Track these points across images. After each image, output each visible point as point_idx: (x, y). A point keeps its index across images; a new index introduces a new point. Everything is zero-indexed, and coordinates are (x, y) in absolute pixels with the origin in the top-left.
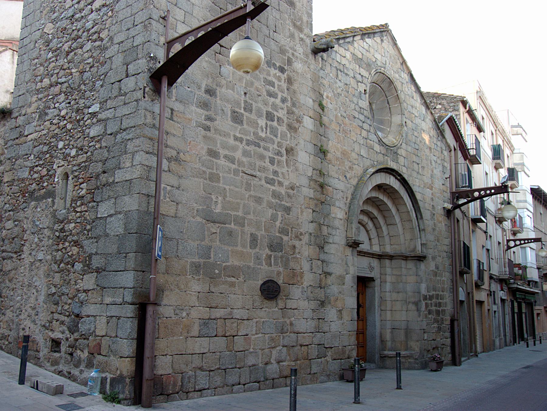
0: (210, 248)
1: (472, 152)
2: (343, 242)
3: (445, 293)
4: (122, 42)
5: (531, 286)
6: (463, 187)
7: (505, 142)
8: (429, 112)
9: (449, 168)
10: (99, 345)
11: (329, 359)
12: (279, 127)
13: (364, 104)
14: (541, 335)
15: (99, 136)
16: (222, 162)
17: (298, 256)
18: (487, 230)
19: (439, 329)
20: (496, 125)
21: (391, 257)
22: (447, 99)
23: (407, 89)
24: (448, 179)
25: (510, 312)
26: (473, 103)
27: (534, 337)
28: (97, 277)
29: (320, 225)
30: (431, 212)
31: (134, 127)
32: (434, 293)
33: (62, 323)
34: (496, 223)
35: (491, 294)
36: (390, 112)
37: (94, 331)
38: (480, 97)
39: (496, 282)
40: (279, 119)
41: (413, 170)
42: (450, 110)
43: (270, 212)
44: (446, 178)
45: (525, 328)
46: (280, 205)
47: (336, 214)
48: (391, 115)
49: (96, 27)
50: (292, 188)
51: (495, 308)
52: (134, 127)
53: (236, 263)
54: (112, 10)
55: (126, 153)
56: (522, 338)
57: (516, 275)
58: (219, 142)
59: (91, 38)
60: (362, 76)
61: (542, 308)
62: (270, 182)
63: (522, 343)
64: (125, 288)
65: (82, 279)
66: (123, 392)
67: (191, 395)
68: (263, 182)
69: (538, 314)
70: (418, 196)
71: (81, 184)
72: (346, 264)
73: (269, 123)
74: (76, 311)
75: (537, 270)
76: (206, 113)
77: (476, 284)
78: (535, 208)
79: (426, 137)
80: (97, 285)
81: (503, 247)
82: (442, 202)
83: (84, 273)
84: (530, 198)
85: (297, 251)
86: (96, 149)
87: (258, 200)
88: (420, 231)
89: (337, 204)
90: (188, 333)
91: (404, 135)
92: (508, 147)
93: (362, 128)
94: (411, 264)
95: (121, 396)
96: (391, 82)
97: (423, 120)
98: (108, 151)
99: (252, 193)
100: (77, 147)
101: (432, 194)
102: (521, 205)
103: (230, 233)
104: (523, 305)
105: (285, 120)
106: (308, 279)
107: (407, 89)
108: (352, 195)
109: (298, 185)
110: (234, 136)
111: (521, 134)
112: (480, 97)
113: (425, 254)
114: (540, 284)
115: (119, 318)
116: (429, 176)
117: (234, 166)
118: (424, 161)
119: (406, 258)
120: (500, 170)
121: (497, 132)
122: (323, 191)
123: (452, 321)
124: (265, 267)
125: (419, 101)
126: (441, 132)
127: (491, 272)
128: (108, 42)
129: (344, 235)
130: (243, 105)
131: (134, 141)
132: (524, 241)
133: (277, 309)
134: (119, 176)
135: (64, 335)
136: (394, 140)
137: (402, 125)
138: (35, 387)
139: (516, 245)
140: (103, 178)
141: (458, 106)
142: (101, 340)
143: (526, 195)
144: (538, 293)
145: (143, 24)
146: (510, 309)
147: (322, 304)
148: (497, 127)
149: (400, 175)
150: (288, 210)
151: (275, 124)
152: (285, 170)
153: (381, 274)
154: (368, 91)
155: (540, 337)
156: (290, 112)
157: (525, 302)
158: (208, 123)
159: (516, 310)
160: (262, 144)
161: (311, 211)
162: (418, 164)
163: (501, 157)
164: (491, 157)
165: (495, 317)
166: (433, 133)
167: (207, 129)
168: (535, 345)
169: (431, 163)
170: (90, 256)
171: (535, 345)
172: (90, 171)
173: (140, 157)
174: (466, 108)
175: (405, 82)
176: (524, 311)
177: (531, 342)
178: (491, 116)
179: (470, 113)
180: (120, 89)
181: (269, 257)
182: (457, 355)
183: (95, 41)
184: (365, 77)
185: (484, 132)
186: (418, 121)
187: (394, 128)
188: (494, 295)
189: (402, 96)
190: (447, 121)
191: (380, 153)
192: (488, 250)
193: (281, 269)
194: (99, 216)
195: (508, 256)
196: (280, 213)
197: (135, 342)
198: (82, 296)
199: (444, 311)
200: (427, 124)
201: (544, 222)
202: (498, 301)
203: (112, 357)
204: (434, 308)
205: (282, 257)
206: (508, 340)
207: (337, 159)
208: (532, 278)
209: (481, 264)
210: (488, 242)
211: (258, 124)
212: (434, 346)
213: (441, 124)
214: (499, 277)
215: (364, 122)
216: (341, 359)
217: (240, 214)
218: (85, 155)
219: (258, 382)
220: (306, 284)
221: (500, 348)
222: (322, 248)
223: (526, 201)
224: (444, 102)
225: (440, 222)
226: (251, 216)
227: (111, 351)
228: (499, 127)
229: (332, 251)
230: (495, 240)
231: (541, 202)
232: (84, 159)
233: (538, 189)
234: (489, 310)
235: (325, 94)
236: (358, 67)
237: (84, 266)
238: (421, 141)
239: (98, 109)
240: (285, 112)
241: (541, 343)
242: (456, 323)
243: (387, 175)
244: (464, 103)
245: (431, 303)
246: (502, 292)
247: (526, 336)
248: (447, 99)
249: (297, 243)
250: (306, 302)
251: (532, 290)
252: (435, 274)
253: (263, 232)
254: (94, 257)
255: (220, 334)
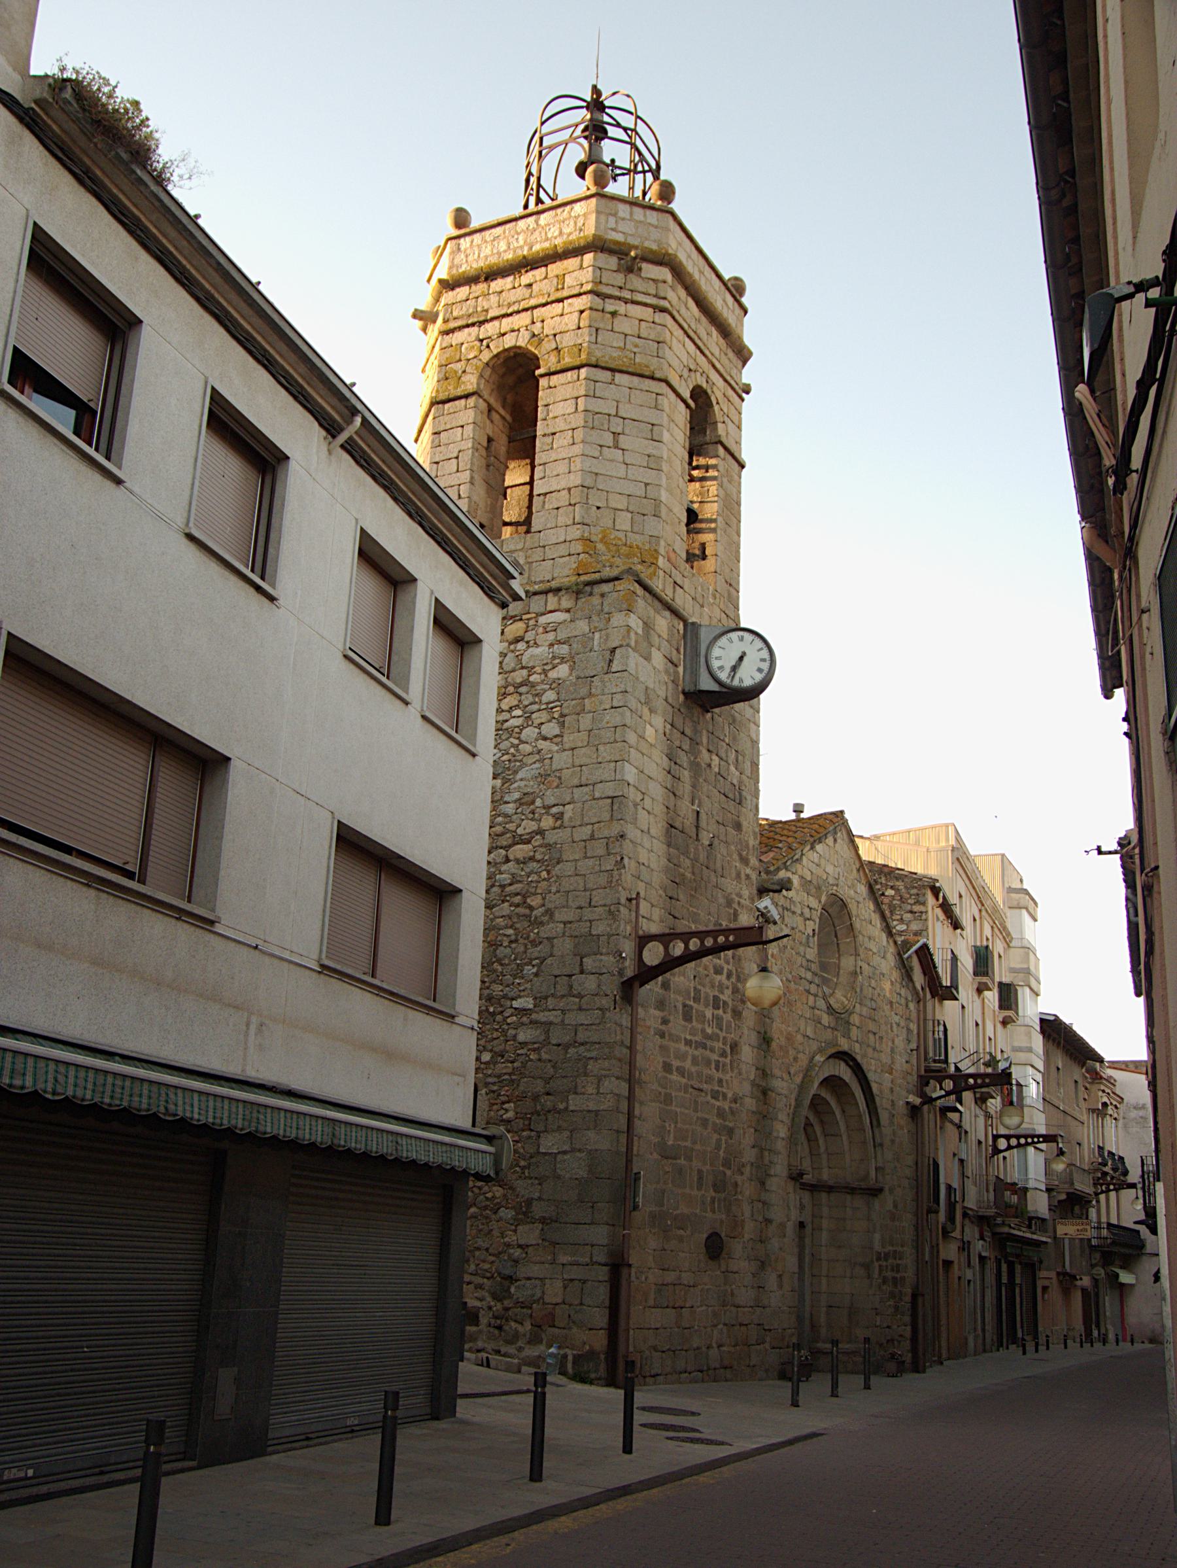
0: (663, 1192)
1: (946, 981)
2: (785, 1173)
3: (905, 1249)
4: (570, 922)
5: (1033, 1227)
6: (935, 1061)
7: (996, 930)
8: (891, 941)
9: (915, 1032)
10: (552, 1315)
11: (767, 1346)
12: (724, 1016)
13: (812, 953)
14: (1049, 1334)
15: (535, 1043)
16: (675, 1077)
17: (740, 1197)
18: (961, 1121)
19: (896, 1308)
20: (981, 902)
21: (830, 1189)
22: (906, 880)
23: (863, 912)
24: (915, 1052)
25: (994, 1283)
26: (953, 888)
27: (1036, 1337)
28: (542, 1230)
29: (762, 1150)
30: (890, 1113)
31: (599, 1043)
32: (891, 1248)
33: (480, 1287)
34: (976, 1103)
35: (965, 1246)
36: (839, 951)
37: (542, 1298)
38: (958, 859)
39: (972, 1222)
40: (725, 1003)
41: (868, 1046)
42: (909, 901)
43: (716, 1136)
44: (912, 1050)
45: (1018, 1318)
46: (725, 1127)
47: (778, 1132)
48: (839, 956)
49: (516, 886)
50: (735, 1101)
51: (969, 1274)
52: (599, 1043)
53: (686, 1211)
54: (548, 872)
55: (586, 1075)
56: (1014, 1340)
57: (1008, 1206)
58: (672, 1050)
59: (508, 898)
60: (811, 909)
61: (1053, 1275)
62: (715, 1095)
63: (1013, 1347)
64: (592, 1246)
65: (515, 1231)
66: (597, 1371)
67: (648, 1380)
68: (709, 1097)
69: (1045, 1288)
70: (875, 1088)
71: (503, 1103)
72: (788, 1206)
73: (716, 1012)
74: (507, 1272)
75: (1046, 1195)
76: (662, 1014)
77: (944, 1228)
78: (1047, 1053)
79: (887, 986)
80: (543, 1240)
81: (986, 1149)
82: (904, 1093)
83: (517, 1222)
84: (1038, 1041)
85: (739, 1190)
86: (531, 1060)
87: (704, 1123)
88: (875, 1147)
89: (780, 1117)
90: (646, 1301)
91: (858, 990)
92: (1001, 937)
93: (808, 992)
94: (859, 1202)
95: (593, 1376)
96: (844, 905)
97: (883, 957)
98: (553, 1067)
99: (699, 1114)
100: (491, 1051)
101: (892, 1082)
102: (1022, 1057)
103: (680, 1171)
104: (1018, 1268)
105: (730, 1003)
106: (749, 1230)
107: (863, 912)
108: (796, 1100)
109: (741, 1095)
110: (685, 1039)
111: (1027, 909)
112: (958, 859)
113: (881, 1185)
114: (1051, 1222)
115: (584, 1282)
116: (889, 1050)
117: (684, 1081)
118: (883, 1027)
119: (852, 1190)
120: (986, 993)
121: (984, 913)
122: (765, 1099)
123: (914, 1296)
124: (709, 1215)
125: (879, 925)
126: (907, 971)
127: (966, 1205)
128: (543, 915)
129: (786, 1163)
130: (692, 995)
131: (599, 1061)
132: (1026, 1139)
133: (718, 1273)
134: (574, 1103)
135: (484, 1303)
136: (844, 999)
137: (856, 973)
138: (485, 1364)
139: (1009, 1147)
140: (548, 1102)
141: (924, 895)
142: (554, 1309)
143: (1030, 1037)
144: (1046, 1243)
145: (607, 908)
146: (994, 1276)
147: (763, 1265)
148: (983, 905)
149: (854, 1060)
150: (730, 1132)
151: (721, 1012)
152: (728, 1077)
153: (813, 1216)
154: (817, 931)
155: (1047, 1336)
156: (736, 991)
157: (1021, 1263)
158: (663, 1027)
159: (1005, 1280)
160: (709, 1043)
161: (752, 1130)
162: (875, 1034)
163: (990, 972)
164: (971, 971)
165: (969, 1292)
166: (895, 975)
167: (662, 1035)
168: (1037, 1351)
169: (892, 1027)
170: (529, 1202)
171: (1037, 1351)
172: (521, 1088)
173: (609, 1085)
174: (937, 899)
175: (861, 899)
176: (1018, 1281)
177: (1030, 1346)
178: (974, 888)
179: (946, 908)
180: (571, 987)
181: (713, 1200)
182: (920, 1353)
183: (517, 906)
184: (814, 909)
185: (963, 929)
186: (876, 960)
187: (843, 979)
188: (969, 1248)
189: (857, 925)
190: (916, 952)
191: (829, 1027)
192: (962, 1161)
193: (724, 1216)
194: (542, 1150)
195: (993, 1170)
196: (723, 1138)
197: (607, 1311)
198: (517, 1253)
199: (903, 1279)
200: (887, 964)
201: (1064, 1086)
202: (975, 1261)
203: (575, 1330)
204: (889, 1274)
205: (725, 1199)
206: (988, 1341)
207: (781, 1047)
208: (1036, 1211)
209: (953, 1191)
210: (963, 1145)
211: (705, 1017)
212: (889, 1338)
213: (906, 956)
214: (977, 1211)
215: (811, 983)
216: (780, 1348)
217: (688, 1144)
218: (510, 1065)
219: (701, 1371)
220: (747, 1237)
221: (975, 1355)
222: (763, 1183)
223: (1030, 1050)
224: (899, 884)
225: (902, 1128)
226: (698, 1147)
227: (574, 1322)
228: (987, 903)
229: (774, 1188)
230: (972, 1138)
231: (1059, 1044)
232: (510, 1070)
233: (1055, 1020)
234: (960, 1278)
235: (770, 952)
236: (806, 895)
237: (517, 1214)
238: (879, 995)
239: (531, 1006)
240: (728, 992)
241: (1048, 1348)
242: (920, 1300)
243: (837, 1060)
244: (936, 891)
245: (887, 1266)
246: (981, 1242)
247: (1020, 1335)
248: (906, 880)
249: (739, 1179)
250: (746, 1263)
251: (1035, 1237)
252: (893, 1219)
253: (708, 1167)
254: (535, 1203)
255: (671, 1305)
